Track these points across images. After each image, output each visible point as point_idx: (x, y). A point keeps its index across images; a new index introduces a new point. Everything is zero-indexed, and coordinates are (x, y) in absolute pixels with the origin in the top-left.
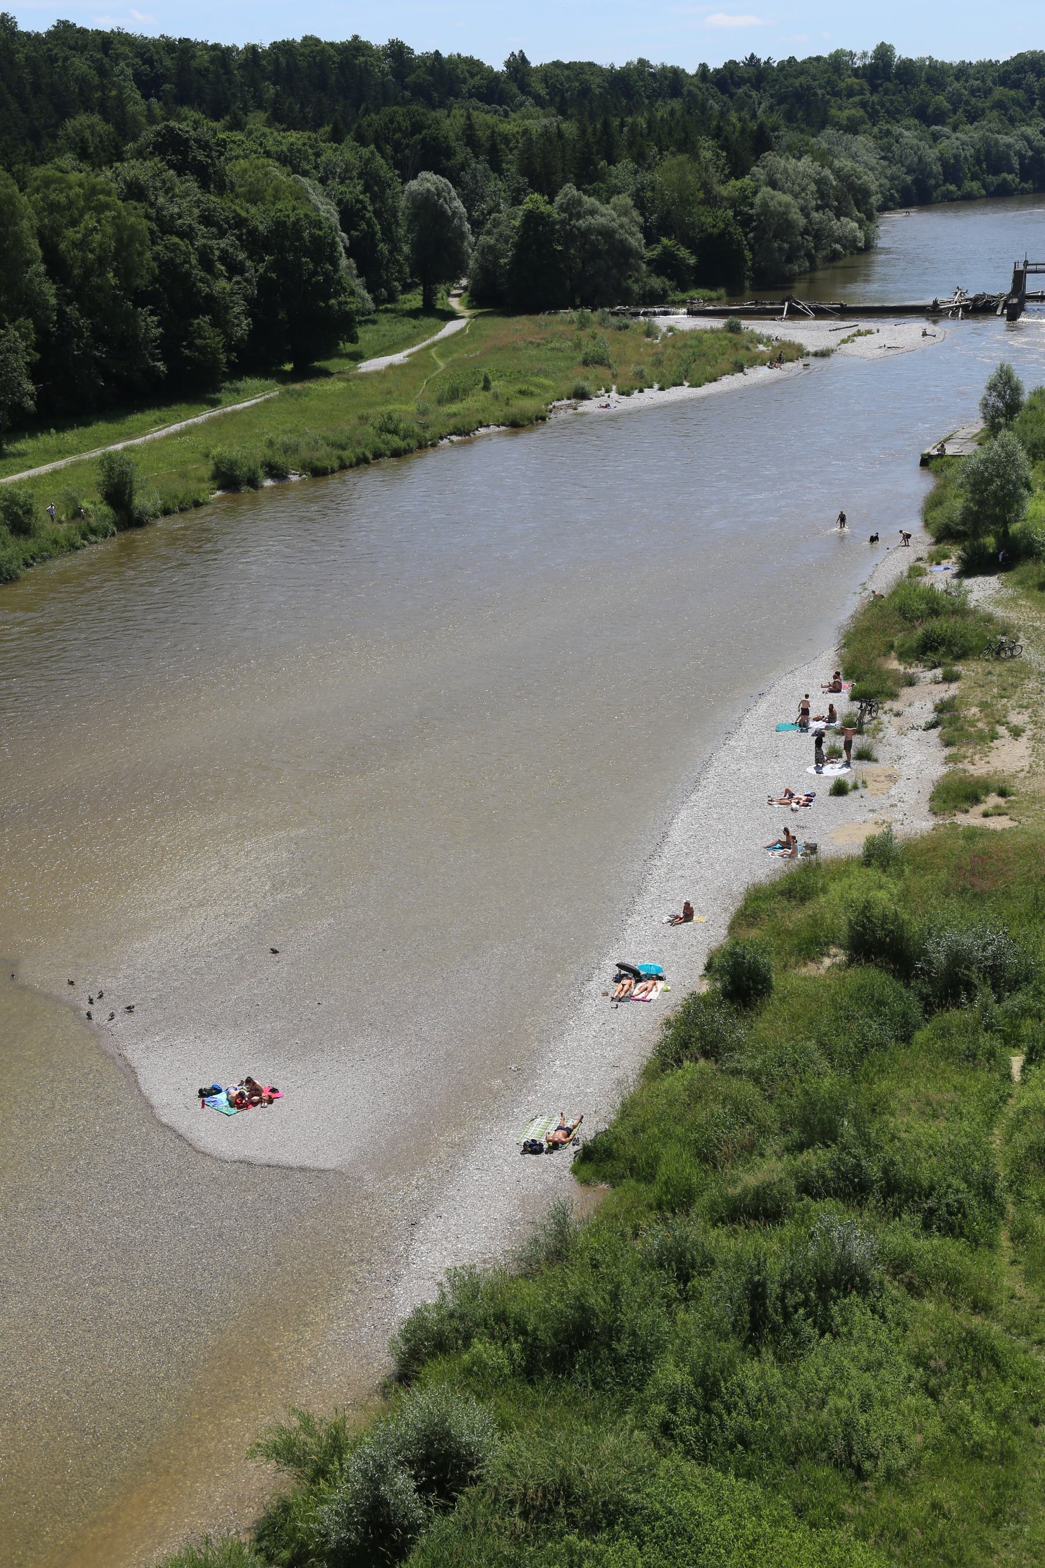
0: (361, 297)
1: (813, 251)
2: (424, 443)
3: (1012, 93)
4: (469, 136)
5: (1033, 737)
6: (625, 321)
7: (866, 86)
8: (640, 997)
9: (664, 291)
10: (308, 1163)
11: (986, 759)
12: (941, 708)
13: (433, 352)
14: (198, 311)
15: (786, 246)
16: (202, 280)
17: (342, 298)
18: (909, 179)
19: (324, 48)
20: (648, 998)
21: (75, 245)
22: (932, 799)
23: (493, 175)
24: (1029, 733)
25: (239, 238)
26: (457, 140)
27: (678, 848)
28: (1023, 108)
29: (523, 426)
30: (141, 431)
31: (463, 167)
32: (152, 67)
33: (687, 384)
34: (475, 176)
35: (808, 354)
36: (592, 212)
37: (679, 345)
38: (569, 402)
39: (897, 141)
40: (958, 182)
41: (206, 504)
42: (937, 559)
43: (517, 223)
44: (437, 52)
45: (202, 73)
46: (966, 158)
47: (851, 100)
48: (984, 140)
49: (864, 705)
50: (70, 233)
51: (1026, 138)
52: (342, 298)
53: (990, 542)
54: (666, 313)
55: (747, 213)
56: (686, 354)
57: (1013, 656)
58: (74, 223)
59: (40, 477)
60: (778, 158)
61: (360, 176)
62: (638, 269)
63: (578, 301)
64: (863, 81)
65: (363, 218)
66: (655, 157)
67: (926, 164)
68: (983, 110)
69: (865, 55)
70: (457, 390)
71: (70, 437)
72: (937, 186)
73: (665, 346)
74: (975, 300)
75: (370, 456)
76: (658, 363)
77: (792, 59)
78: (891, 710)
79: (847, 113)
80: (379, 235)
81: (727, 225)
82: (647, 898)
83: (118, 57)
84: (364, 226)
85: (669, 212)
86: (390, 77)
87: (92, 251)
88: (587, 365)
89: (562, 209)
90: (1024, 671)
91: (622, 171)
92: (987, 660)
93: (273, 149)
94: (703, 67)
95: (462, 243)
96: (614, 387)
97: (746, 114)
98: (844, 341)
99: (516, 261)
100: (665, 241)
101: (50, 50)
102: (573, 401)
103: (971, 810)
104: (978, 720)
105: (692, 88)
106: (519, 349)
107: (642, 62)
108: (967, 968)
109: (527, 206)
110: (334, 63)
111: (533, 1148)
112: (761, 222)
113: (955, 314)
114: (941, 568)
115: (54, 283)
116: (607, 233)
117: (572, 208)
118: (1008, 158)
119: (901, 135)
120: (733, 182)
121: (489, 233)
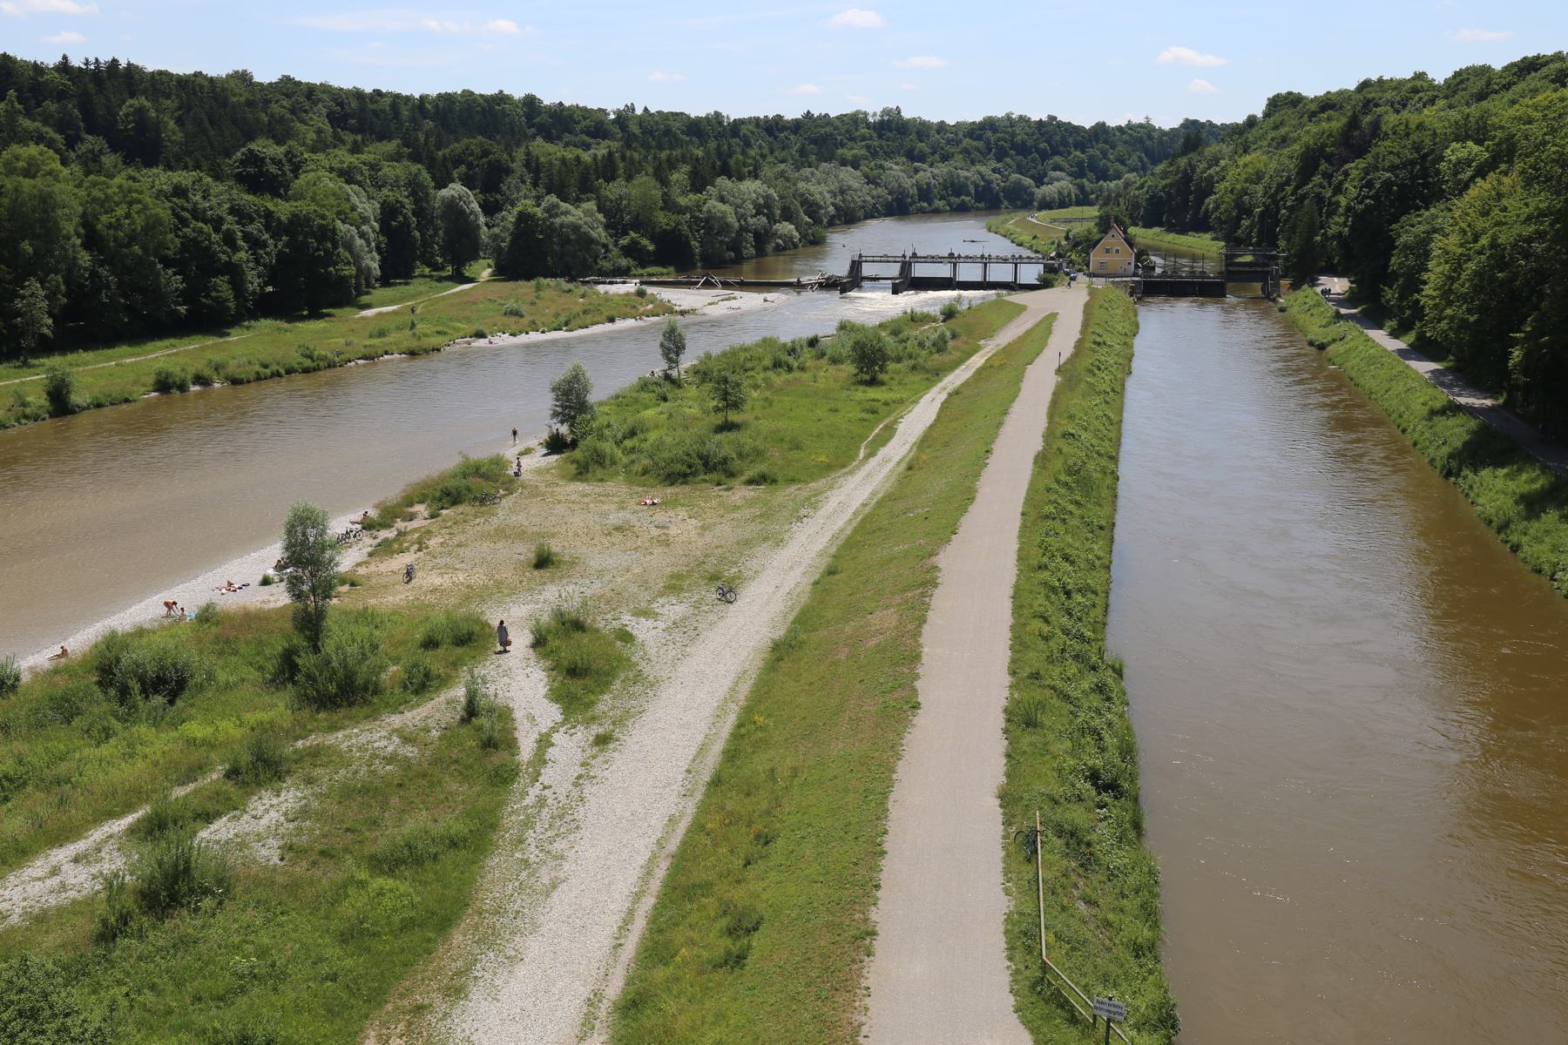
3: (975, 143)
14: (218, 272)
18: (890, 197)
21: (110, 226)
30: (152, 352)
32: (342, 108)
36: (566, 213)
51: (980, 173)
54: (624, 283)
64: (872, 132)
65: (401, 213)
67: (904, 188)
68: (953, 154)
69: (875, 114)
72: (913, 202)
75: (283, 372)
84: (401, 219)
89: (547, 210)
99: (513, 242)
101: (266, 95)
107: (717, 114)
116: (576, 228)
117: (552, 211)
120: (691, 196)
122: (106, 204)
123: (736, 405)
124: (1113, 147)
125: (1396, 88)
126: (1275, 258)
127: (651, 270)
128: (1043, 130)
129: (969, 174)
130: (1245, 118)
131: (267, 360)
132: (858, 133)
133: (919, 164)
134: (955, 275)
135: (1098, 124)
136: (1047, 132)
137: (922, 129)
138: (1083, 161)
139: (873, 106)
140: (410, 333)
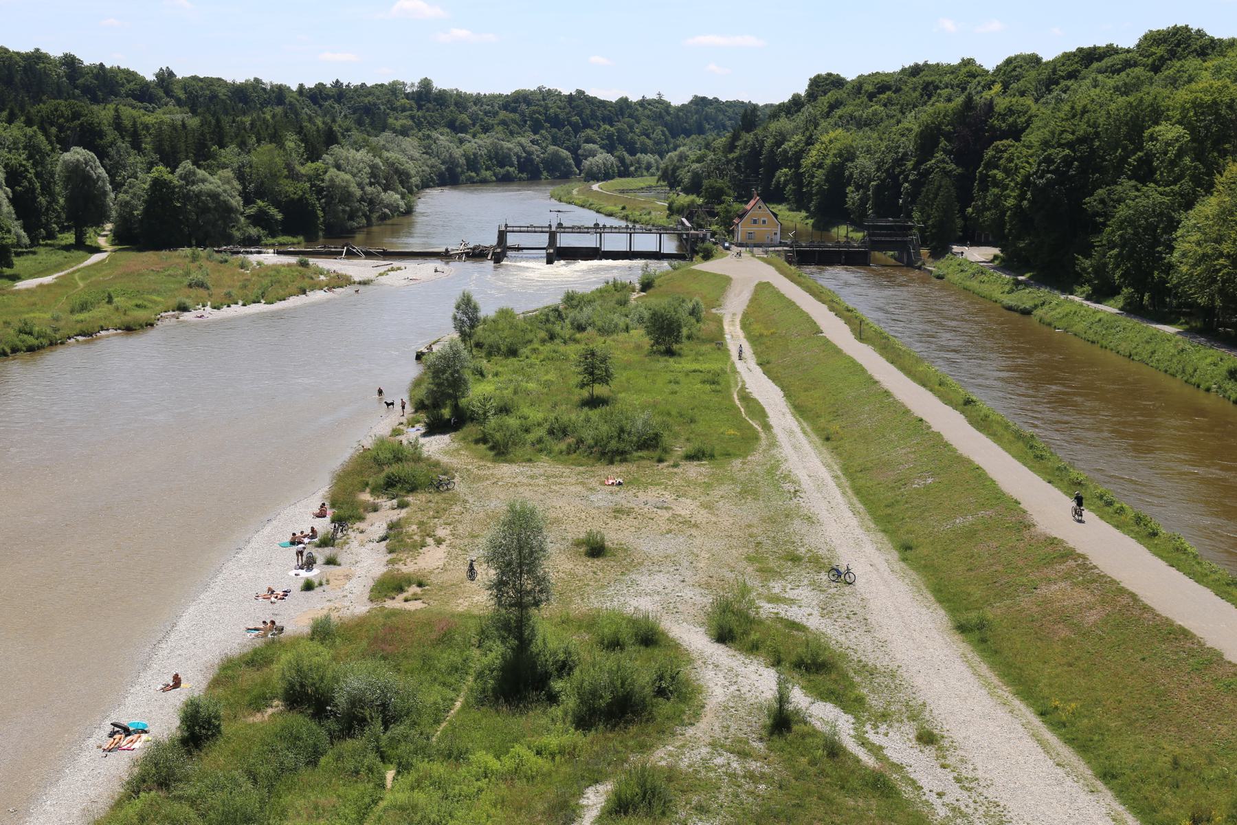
1: (368, 213)
2: (54, 342)
3: (511, 115)
4: (117, 124)
6: (225, 256)
7: (414, 105)
8: (125, 747)
9: (259, 237)
11: (415, 561)
12: (391, 527)
13: (76, 276)
15: (348, 209)
18: (443, 167)
19: (12, 56)
20: (132, 748)
22: (371, 591)
23: (133, 152)
24: (448, 542)
26: (109, 126)
27: (181, 634)
28: (519, 125)
29: (135, 330)
31: (112, 144)
33: (263, 301)
34: (119, 151)
35: (354, 283)
36: (203, 181)
37: (262, 274)
38: (173, 313)
39: (435, 142)
40: (476, 170)
42: (412, 423)
43: (146, 186)
44: (101, 64)
46: (481, 155)
47: (404, 114)
48: (494, 145)
49: (337, 525)
51: (521, 145)
53: (446, 412)
54: (259, 253)
55: (319, 186)
56: (266, 282)
57: (448, 489)
60: (341, 150)
61: (25, 148)
62: (237, 221)
63: (194, 242)
64: (412, 102)
65: (25, 177)
66: (253, 145)
67: (454, 158)
68: (493, 125)
69: (413, 85)
70: (86, 303)
72: (463, 172)
73: (253, 275)
74: (474, 249)
75: (8, 351)
77: (363, 85)
78: (358, 529)
79: (400, 122)
81: (304, 193)
82: (150, 672)
84: (26, 183)
85: (262, 183)
86: (64, 79)
88: (191, 288)
89: (181, 177)
90: (454, 499)
91: (230, 154)
92: (430, 493)
94: (301, 86)
95: (105, 198)
96: (209, 303)
97: (328, 119)
98: (381, 274)
99: (146, 211)
100: (260, 203)
102: (177, 312)
103: (397, 597)
104: (415, 534)
105: (292, 99)
106: (142, 275)
108: (362, 708)
109: (155, 173)
110: (20, 66)
112: (330, 192)
113: (460, 258)
114: (414, 429)
116: (214, 196)
117: (188, 178)
118: (509, 157)
119: (438, 138)
120: (309, 164)
121: (126, 192)
123: (605, 379)
124: (638, 123)
125: (952, 73)
126: (911, 228)
127: (282, 239)
128: (574, 104)
129: (511, 145)
130: (790, 97)
132: (399, 104)
133: (463, 135)
134: (601, 245)
136: (577, 106)
137: (461, 101)
138: (613, 134)
139: (411, 79)
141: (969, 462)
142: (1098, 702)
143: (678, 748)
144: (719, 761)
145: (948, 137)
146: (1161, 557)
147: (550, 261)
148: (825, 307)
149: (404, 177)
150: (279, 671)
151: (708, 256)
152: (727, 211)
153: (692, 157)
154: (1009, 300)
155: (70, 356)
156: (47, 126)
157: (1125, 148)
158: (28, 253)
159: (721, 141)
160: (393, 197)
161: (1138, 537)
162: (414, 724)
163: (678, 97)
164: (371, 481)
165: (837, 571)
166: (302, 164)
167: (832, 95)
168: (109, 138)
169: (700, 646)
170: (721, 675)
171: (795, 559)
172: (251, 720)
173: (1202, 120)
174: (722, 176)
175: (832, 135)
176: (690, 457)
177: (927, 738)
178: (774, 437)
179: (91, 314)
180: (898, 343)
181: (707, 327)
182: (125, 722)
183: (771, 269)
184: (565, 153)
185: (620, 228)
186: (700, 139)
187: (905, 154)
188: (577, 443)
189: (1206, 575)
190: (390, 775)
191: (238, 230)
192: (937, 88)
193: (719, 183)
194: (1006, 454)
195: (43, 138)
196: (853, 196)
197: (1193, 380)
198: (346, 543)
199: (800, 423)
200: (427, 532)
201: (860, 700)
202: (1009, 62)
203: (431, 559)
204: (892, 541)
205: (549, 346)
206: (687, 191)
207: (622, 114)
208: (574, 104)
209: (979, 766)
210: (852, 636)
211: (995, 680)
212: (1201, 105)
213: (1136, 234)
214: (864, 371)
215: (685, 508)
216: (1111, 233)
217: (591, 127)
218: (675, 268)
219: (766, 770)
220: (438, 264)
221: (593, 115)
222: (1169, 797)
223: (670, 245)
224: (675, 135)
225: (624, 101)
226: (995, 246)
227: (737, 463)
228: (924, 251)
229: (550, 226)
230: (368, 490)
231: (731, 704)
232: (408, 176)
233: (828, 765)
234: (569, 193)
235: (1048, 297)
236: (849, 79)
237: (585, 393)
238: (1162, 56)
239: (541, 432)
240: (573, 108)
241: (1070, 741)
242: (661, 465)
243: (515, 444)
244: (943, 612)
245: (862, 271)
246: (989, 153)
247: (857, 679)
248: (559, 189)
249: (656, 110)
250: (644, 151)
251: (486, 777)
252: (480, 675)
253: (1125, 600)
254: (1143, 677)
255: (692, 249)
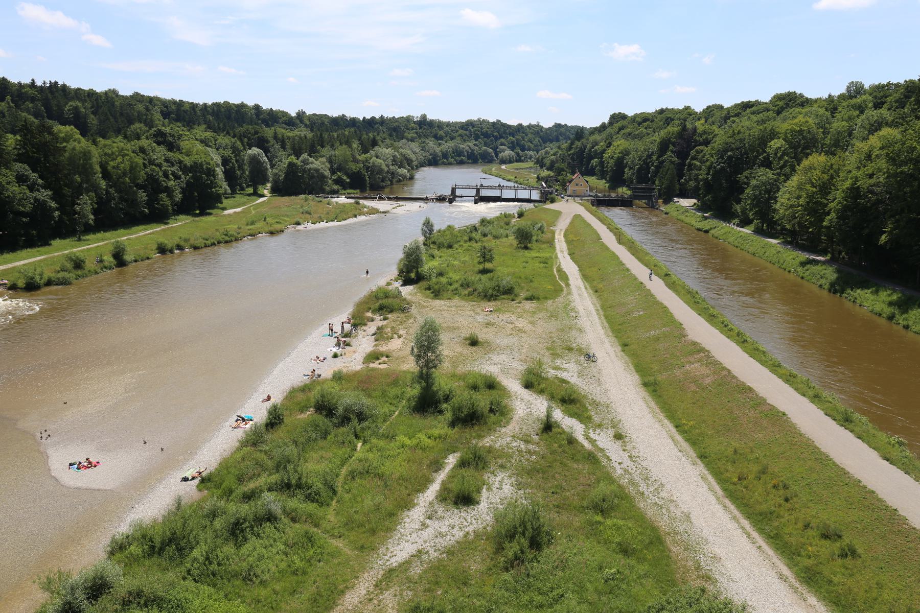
0: (225, 186)
4: (275, 137)
5: (406, 339)
6: (320, 199)
7: (418, 127)
9: (338, 190)
10: (101, 487)
12: (378, 329)
13: (252, 208)
16: (164, 181)
17: (217, 189)
21: (114, 167)
25: (180, 167)
30: (136, 233)
32: (167, 109)
36: (312, 163)
41: (151, 258)
42: (396, 280)
43: (286, 166)
45: (185, 112)
50: (112, 163)
52: (217, 189)
53: (413, 275)
54: (338, 197)
57: (408, 312)
58: (114, 160)
59: (91, 248)
61: (231, 148)
62: (328, 182)
63: (307, 192)
69: (417, 117)
71: (108, 234)
72: (440, 159)
74: (440, 196)
75: (216, 243)
76: (328, 213)
79: (411, 135)
80: (237, 168)
82: (258, 393)
83: (155, 105)
84: (231, 165)
85: (341, 164)
87: (120, 170)
89: (302, 162)
90: (410, 317)
91: (326, 151)
93: (199, 138)
97: (375, 134)
98: (393, 208)
99: (286, 178)
100: (339, 173)
111: (185, 479)
115: (105, 180)
116: (317, 170)
117: (305, 162)
120: (363, 155)
121: (277, 169)
122: (112, 156)
124: (527, 136)
126: (654, 189)
128: (495, 126)
129: (464, 146)
131: (207, 237)
135: (519, 124)
136: (497, 128)
137: (440, 125)
139: (416, 114)
140: (265, 223)
141: (662, 304)
142: (704, 421)
143: (496, 437)
144: (515, 444)
145: (674, 144)
146: (747, 353)
147: (476, 203)
148: (605, 227)
149: (409, 161)
150: (314, 395)
151: (553, 201)
152: (564, 179)
153: (552, 153)
154: (699, 225)
155: (247, 243)
156: (242, 138)
157: (758, 152)
158: (231, 197)
159: (565, 146)
160: (404, 171)
161: (737, 343)
162: (374, 422)
163: (547, 124)
164: (372, 307)
165: (589, 355)
166: (360, 155)
167: (619, 124)
168: (271, 144)
169: (516, 390)
170: (523, 404)
171: (570, 349)
172: (299, 417)
173: (795, 138)
174: (563, 162)
175: (619, 143)
176: (527, 299)
177: (618, 437)
178: (571, 290)
179: (255, 226)
180: (639, 245)
181: (547, 236)
182: (243, 415)
183: (582, 208)
184: (490, 150)
185: (511, 187)
186: (557, 144)
187: (653, 153)
188: (474, 291)
189: (767, 362)
190: (359, 445)
191: (328, 186)
192: (673, 120)
193: (562, 166)
194: (681, 301)
195: (239, 143)
196: (628, 173)
197: (783, 267)
198: (356, 336)
199: (584, 283)
200: (394, 331)
201: (589, 418)
202: (709, 107)
203: (394, 345)
204: (619, 342)
205: (468, 244)
206: (548, 169)
207: (519, 131)
208: (495, 126)
209: (641, 451)
210: (591, 387)
211: (657, 410)
212: (795, 131)
213: (760, 194)
214: (618, 258)
215: (522, 323)
216: (749, 191)
217: (504, 138)
218: (536, 207)
219: (537, 449)
220: (422, 204)
221: (505, 132)
222: (730, 467)
223: (535, 195)
224: (545, 142)
225: (520, 125)
226: (693, 198)
227: (550, 302)
228: (660, 201)
229: (477, 186)
230: (371, 311)
231: (526, 418)
232: (412, 161)
233: (567, 448)
234: (491, 169)
235: (718, 224)
236: (629, 116)
237: (481, 267)
238: (782, 107)
239: (456, 285)
240: (495, 128)
241: (687, 440)
242: (512, 302)
243: (443, 290)
244: (638, 377)
245: (628, 209)
246: (693, 153)
247: (590, 408)
248: (486, 167)
249: (536, 130)
250: (529, 150)
251: (403, 447)
252: (409, 400)
253: (724, 373)
254: (727, 410)
255: (547, 198)
